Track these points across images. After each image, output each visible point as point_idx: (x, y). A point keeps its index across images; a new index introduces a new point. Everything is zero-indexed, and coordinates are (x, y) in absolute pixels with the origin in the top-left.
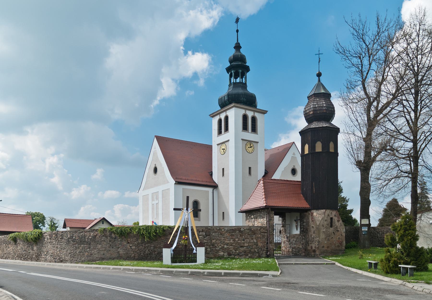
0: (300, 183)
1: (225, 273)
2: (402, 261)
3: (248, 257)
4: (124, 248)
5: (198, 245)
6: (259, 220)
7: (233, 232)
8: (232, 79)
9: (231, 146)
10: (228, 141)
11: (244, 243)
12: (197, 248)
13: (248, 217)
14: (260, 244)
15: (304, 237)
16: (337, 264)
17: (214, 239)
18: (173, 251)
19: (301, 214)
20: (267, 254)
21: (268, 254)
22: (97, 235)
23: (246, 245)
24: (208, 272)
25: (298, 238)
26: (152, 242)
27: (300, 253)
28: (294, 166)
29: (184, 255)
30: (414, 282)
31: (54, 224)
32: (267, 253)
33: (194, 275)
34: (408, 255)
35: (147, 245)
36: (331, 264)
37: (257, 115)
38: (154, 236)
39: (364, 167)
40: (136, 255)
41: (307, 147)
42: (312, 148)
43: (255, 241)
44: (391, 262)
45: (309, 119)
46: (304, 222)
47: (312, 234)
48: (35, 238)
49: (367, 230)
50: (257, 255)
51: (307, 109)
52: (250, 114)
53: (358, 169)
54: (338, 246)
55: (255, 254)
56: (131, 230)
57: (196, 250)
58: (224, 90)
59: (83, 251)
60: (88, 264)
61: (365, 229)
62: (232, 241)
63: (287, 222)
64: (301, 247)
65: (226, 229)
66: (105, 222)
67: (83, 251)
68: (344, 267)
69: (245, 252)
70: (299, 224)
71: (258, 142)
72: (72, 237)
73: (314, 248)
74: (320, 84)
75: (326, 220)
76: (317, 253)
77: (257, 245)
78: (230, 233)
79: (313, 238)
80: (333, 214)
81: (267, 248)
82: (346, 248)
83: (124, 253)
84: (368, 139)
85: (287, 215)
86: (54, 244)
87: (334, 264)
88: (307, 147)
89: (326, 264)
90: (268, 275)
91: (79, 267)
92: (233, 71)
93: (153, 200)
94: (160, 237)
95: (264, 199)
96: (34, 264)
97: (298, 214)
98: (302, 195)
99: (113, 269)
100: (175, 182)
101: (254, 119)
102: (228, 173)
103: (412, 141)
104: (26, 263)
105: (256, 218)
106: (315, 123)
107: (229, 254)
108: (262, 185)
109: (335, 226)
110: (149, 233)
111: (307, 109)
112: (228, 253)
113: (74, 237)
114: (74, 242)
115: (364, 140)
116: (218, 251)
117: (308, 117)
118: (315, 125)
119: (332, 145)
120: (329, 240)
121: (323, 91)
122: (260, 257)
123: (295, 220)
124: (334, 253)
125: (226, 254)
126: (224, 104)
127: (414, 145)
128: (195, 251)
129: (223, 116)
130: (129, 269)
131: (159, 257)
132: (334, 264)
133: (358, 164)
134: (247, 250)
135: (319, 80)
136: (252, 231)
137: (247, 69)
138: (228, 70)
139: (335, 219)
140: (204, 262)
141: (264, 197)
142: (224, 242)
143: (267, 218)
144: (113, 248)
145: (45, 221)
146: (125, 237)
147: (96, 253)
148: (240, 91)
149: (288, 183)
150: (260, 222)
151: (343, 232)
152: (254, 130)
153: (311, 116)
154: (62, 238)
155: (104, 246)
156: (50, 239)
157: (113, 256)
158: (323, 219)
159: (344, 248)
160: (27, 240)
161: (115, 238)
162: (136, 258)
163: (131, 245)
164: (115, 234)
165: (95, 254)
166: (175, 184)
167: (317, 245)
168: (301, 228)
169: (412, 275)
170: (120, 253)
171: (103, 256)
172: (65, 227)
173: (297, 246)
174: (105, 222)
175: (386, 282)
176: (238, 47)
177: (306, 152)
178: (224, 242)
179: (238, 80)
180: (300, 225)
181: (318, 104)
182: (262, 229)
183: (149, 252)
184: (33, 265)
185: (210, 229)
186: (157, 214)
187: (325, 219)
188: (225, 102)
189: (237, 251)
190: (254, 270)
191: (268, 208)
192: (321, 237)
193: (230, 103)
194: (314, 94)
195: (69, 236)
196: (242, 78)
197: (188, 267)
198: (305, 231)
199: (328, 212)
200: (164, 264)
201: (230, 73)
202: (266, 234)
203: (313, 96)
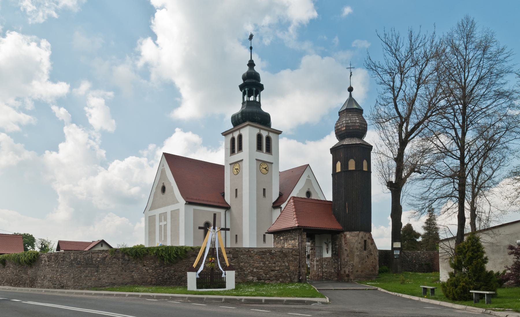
1: (266, 300)
2: (472, 287)
3: (279, 282)
4: (139, 272)
5: (226, 268)
6: (290, 242)
7: (263, 254)
8: (246, 97)
9: (245, 166)
11: (275, 267)
12: (226, 272)
14: (292, 268)
16: (379, 289)
17: (242, 262)
18: (199, 274)
20: (299, 279)
22: (106, 257)
23: (277, 268)
24: (245, 299)
25: (329, 261)
26: (172, 265)
27: (332, 277)
28: (309, 189)
29: (211, 279)
30: (499, 311)
31: (45, 247)
33: (228, 302)
34: (477, 280)
35: (166, 268)
36: (373, 289)
37: (271, 135)
38: (175, 258)
39: (396, 188)
40: (153, 280)
41: (339, 164)
42: (345, 165)
43: (287, 264)
44: (459, 287)
45: (340, 135)
46: (336, 245)
47: (345, 257)
48: (30, 261)
50: (289, 280)
51: (338, 125)
52: (264, 134)
53: (389, 190)
54: (372, 271)
55: (286, 278)
56: (148, 251)
57: (225, 274)
58: (237, 108)
59: (89, 275)
60: (96, 290)
63: (317, 245)
64: (333, 271)
65: (256, 251)
66: (104, 245)
67: (89, 275)
68: (389, 292)
70: (330, 247)
71: (272, 163)
72: (77, 258)
73: (347, 272)
74: (351, 100)
75: (360, 243)
76: (352, 277)
77: (289, 269)
78: (259, 255)
79: (347, 262)
81: (299, 273)
83: (139, 277)
84: (399, 159)
85: (317, 237)
86: (53, 267)
87: (377, 289)
88: (339, 164)
89: (368, 289)
90: (316, 302)
91: (86, 294)
92: (246, 89)
93: (160, 221)
94: (181, 259)
95: (295, 219)
96: (22, 290)
99: (129, 295)
100: (185, 202)
101: (268, 139)
102: (242, 194)
103: (459, 159)
104: (18, 289)
105: (286, 240)
106: (347, 139)
107: (259, 279)
110: (169, 255)
113: (79, 260)
114: (78, 264)
115: (396, 160)
116: (246, 275)
117: (340, 134)
118: (346, 142)
119: (365, 163)
120: (363, 264)
121: (355, 107)
122: (292, 282)
123: (326, 243)
124: (368, 277)
125: (255, 278)
126: (238, 121)
127: (461, 162)
128: (223, 275)
129: (236, 135)
130: (149, 296)
131: (183, 282)
132: (377, 289)
133: (390, 185)
135: (351, 95)
136: (284, 254)
137: (261, 88)
138: (242, 87)
140: (234, 287)
141: (295, 216)
142: (253, 265)
144: (125, 271)
145: (35, 243)
146: (141, 260)
147: (105, 277)
148: (254, 109)
149: (318, 202)
150: (291, 244)
152: (269, 150)
154: (64, 261)
155: (115, 269)
156: (49, 261)
157: (126, 281)
159: (377, 272)
160: (20, 263)
161: (129, 260)
162: (153, 283)
163: (147, 268)
164: (128, 255)
165: (104, 279)
166: (186, 204)
167: (352, 269)
168: (332, 251)
169: (489, 302)
170: (134, 277)
171: (114, 281)
172: (58, 248)
173: (329, 270)
174: (104, 245)
175: (459, 309)
176: (251, 64)
177: (338, 170)
179: (252, 98)
180: (332, 248)
183: (168, 277)
184: (26, 292)
185: (237, 251)
186: (165, 236)
187: (359, 241)
188: (238, 120)
190: (297, 296)
191: (300, 229)
192: (355, 261)
193: (244, 121)
195: (72, 258)
196: (256, 97)
197: (218, 293)
198: (337, 254)
200: (188, 289)
201: (243, 91)
202: (298, 257)
203: (345, 111)
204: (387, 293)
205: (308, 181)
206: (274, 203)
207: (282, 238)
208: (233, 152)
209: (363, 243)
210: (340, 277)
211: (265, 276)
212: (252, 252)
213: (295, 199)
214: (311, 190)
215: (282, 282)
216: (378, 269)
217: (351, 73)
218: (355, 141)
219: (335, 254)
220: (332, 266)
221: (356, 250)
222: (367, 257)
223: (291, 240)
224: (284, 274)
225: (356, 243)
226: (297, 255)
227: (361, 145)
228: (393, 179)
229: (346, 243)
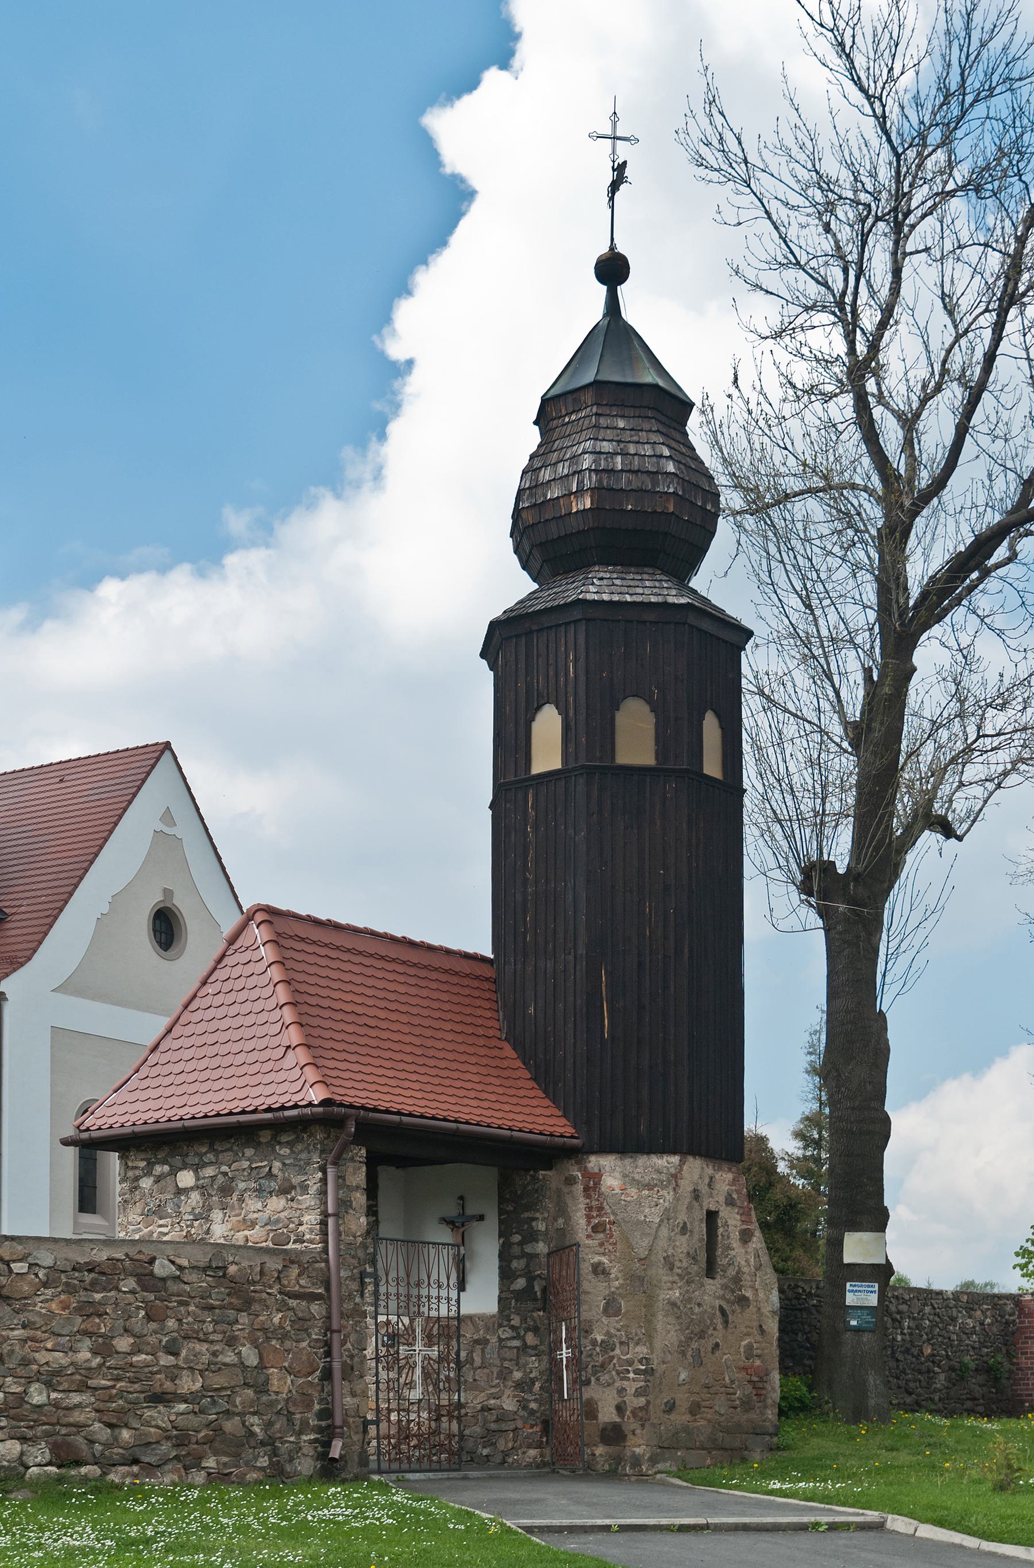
0: (488, 972)
3: (200, 1478)
6: (253, 1204)
7: (93, 1287)
13: (146, 1183)
14: (281, 1384)
15: (530, 1339)
16: (898, 1524)
19: (515, 1172)
20: (323, 1455)
23: (190, 1384)
25: (483, 1342)
27: (501, 1445)
28: (168, 893)
32: (327, 1445)
41: (548, 728)
42: (589, 734)
46: (532, 1237)
49: (873, 1300)
50: (263, 1462)
51: (546, 475)
54: (747, 1405)
55: (248, 1453)
61: (861, 1296)
62: (84, 1355)
65: (46, 1258)
69: (181, 1438)
73: (607, 1414)
74: (614, 334)
75: (684, 1230)
76: (639, 1446)
77: (262, 1389)
78: (70, 1289)
81: (326, 1413)
82: (781, 1413)
87: (879, 1527)
88: (548, 728)
97: (486, 1177)
98: (509, 1051)
107: (66, 1457)
108: (267, 953)
109: (731, 1272)
111: (546, 475)
112: (55, 1448)
118: (599, 587)
119: (711, 727)
120: (698, 1361)
121: (649, 377)
124: (725, 1449)
125: (40, 1453)
132: (879, 1527)
134: (195, 1421)
135: (613, 306)
139: (731, 1220)
143: (323, 1193)
151: (766, 1310)
153: (574, 525)
158: (667, 1216)
159: (771, 1414)
167: (638, 1393)
168: (506, 1275)
178: (26, 1362)
180: (504, 1257)
181: (624, 454)
182: (295, 1271)
187: (682, 1217)
189: (126, 1434)
192: (658, 1344)
194: (596, 384)
198: (538, 1293)
199: (695, 1169)
202: (316, 1308)
203: (589, 397)
204: (978, 1553)
205: (165, 844)
207: (186, 1178)
209: (701, 1229)
210: (565, 1445)
212: (18, 1267)
213: (282, 925)
214: (182, 903)
215: (219, 1478)
216: (776, 1396)
217: (620, 169)
218: (648, 589)
219: (525, 1295)
220: (504, 1375)
221: (659, 1272)
222: (719, 1320)
223: (260, 1192)
224: (231, 1426)
225: (664, 1232)
226: (313, 1297)
227: (692, 619)
228: (840, 849)
229: (596, 1229)
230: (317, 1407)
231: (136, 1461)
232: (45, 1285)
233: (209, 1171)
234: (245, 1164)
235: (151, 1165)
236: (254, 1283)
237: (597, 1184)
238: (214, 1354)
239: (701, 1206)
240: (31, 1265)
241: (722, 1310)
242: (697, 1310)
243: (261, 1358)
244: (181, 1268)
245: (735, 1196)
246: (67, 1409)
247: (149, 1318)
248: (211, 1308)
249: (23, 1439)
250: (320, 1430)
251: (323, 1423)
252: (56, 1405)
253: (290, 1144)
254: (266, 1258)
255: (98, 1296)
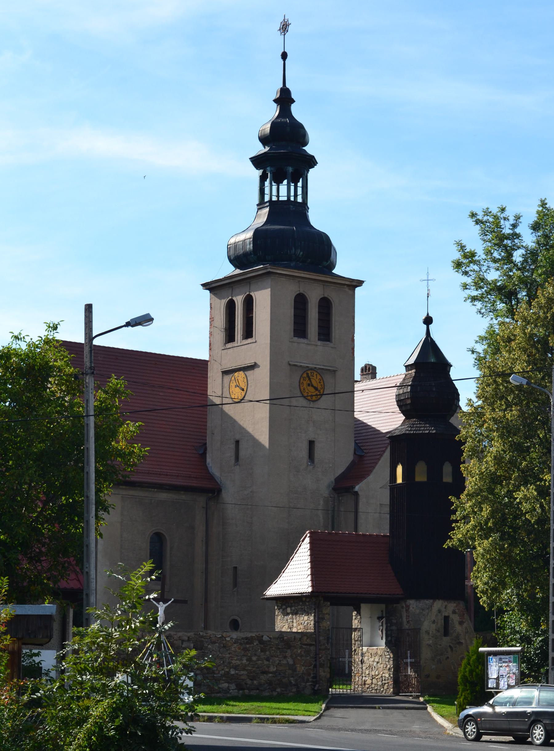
7: (247, 643)
10: (253, 367)
11: (268, 667)
14: (301, 669)
20: (313, 689)
21: (316, 688)
23: (273, 669)
32: (315, 686)
41: (400, 469)
42: (408, 474)
43: (291, 662)
50: (294, 690)
64: (387, 675)
75: (434, 622)
78: (241, 644)
80: (450, 608)
81: (315, 677)
107: (240, 687)
112: (237, 685)
119: (447, 469)
125: (233, 686)
139: (455, 618)
143: (315, 616)
152: (325, 334)
176: (285, 99)
177: (399, 480)
182: (305, 638)
189: (255, 682)
202: (312, 648)
203: (414, 367)
206: (338, 480)
208: (230, 337)
209: (441, 622)
211: (249, 682)
222: (449, 649)
230: (312, 675)
231: (258, 689)
232: (235, 643)
233: (293, 608)
234: (300, 607)
235: (282, 606)
236: (292, 641)
237: (409, 609)
238: (280, 661)
239: (442, 615)
240: (231, 638)
241: (450, 646)
242: (439, 646)
243: (294, 661)
244: (270, 638)
245: (457, 611)
246: (240, 675)
247: (262, 651)
248: (279, 648)
249: (228, 683)
250: (313, 682)
251: (314, 680)
252: (237, 674)
253: (308, 602)
254: (296, 635)
255: (248, 646)
